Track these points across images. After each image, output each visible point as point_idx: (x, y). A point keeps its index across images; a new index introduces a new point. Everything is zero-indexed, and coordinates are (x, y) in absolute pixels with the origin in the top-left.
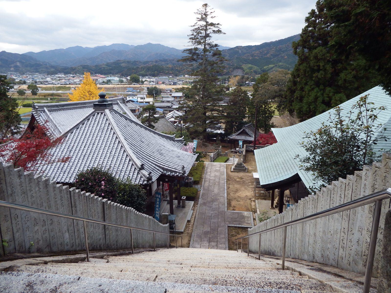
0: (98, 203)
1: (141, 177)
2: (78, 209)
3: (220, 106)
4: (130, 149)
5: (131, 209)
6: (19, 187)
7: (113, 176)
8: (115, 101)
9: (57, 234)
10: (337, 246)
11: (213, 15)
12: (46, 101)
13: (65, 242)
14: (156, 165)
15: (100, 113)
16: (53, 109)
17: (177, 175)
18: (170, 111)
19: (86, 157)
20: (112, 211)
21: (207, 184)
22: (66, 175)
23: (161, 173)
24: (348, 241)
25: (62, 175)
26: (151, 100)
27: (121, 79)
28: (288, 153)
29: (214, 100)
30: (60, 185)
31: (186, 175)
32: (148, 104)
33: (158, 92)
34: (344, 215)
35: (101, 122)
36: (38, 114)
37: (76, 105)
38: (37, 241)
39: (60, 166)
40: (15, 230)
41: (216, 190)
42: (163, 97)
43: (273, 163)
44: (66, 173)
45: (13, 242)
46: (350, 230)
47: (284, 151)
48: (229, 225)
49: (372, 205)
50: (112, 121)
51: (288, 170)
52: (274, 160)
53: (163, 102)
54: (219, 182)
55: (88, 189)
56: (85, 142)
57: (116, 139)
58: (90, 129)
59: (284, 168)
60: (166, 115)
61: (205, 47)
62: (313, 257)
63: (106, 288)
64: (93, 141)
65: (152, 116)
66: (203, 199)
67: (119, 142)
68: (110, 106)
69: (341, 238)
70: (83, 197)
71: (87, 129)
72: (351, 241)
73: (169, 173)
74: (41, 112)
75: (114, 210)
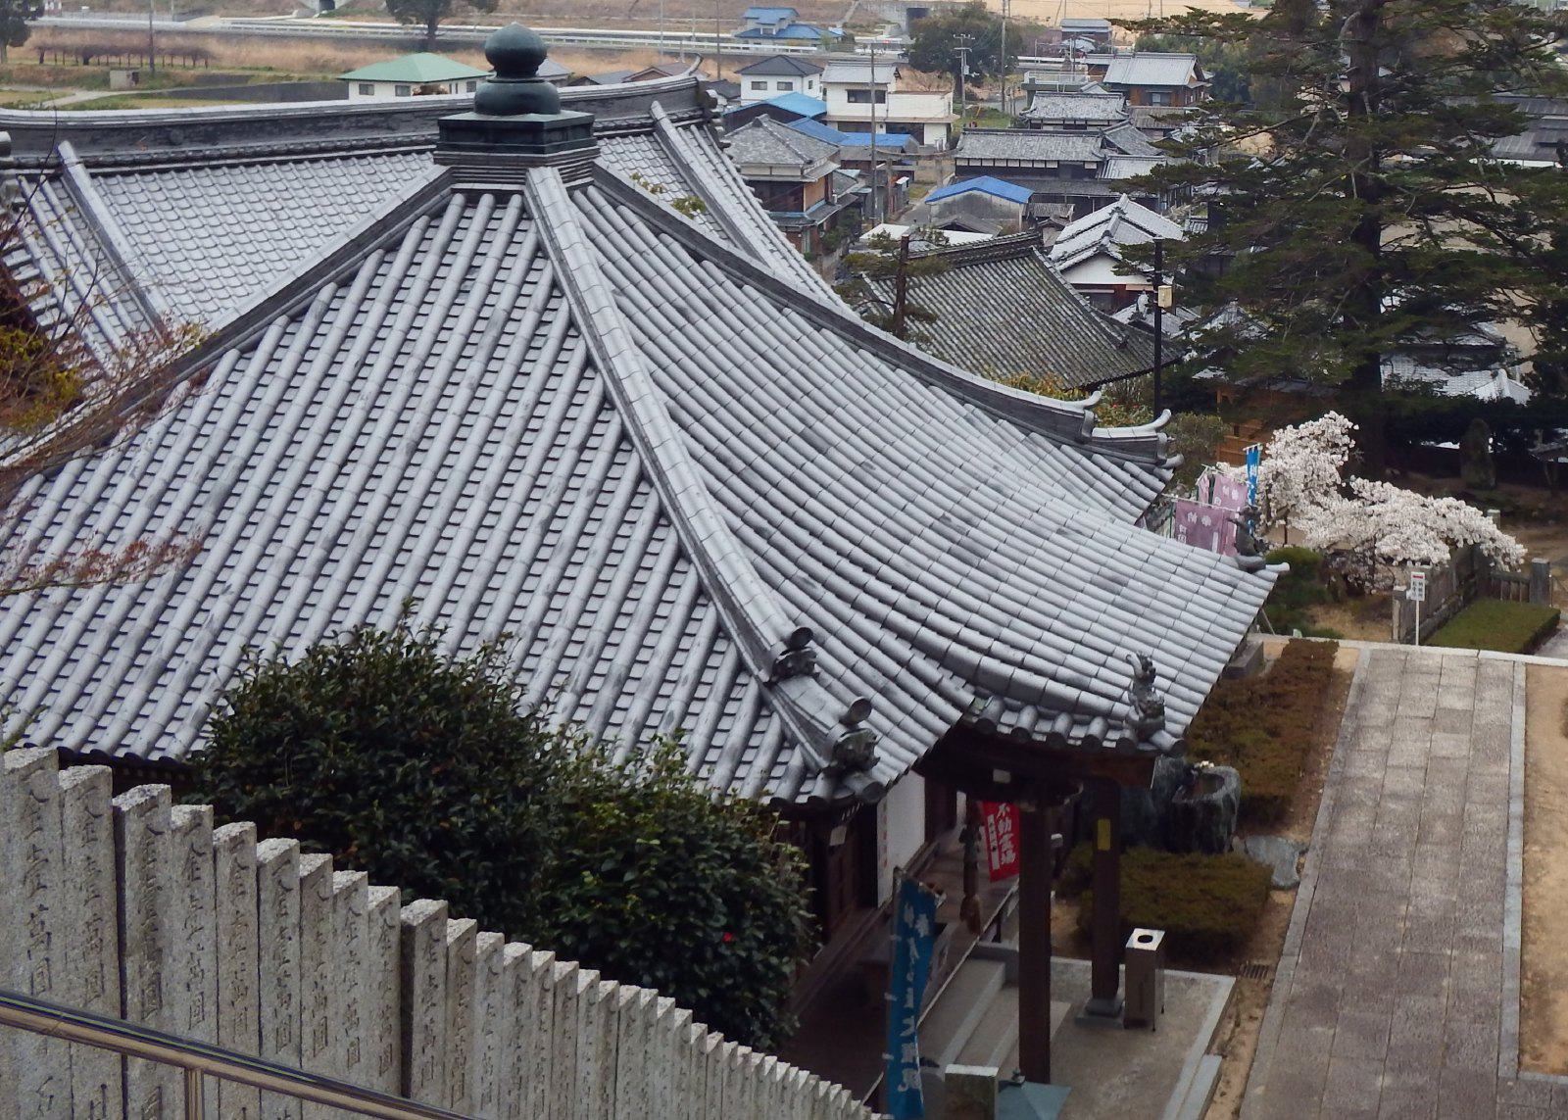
0: (361, 926)
2: (175, 969)
3: (1495, 177)
5: (652, 1004)
7: (523, 713)
8: (628, 110)
12: (94, 95)
14: (916, 643)
15: (487, 201)
16: (125, 152)
17: (1089, 739)
18: (1084, 206)
19: (346, 558)
20: (480, 1011)
21: (1353, 829)
22: (166, 699)
23: (956, 715)
25: (133, 696)
29: (1456, 121)
30: (85, 772)
31: (1166, 739)
32: (903, 139)
33: (994, 45)
35: (487, 266)
37: (319, 131)
39: (125, 618)
41: (1430, 891)
42: (1032, 90)
44: (174, 682)
50: (581, 258)
53: (1032, 127)
54: (1460, 819)
55: (309, 811)
56: (349, 429)
57: (600, 409)
58: (400, 323)
60: (1047, 237)
64: (417, 419)
67: (624, 436)
68: (571, 140)
70: (225, 867)
71: (370, 322)
73: (1025, 719)
74: (31, 179)
75: (495, 999)
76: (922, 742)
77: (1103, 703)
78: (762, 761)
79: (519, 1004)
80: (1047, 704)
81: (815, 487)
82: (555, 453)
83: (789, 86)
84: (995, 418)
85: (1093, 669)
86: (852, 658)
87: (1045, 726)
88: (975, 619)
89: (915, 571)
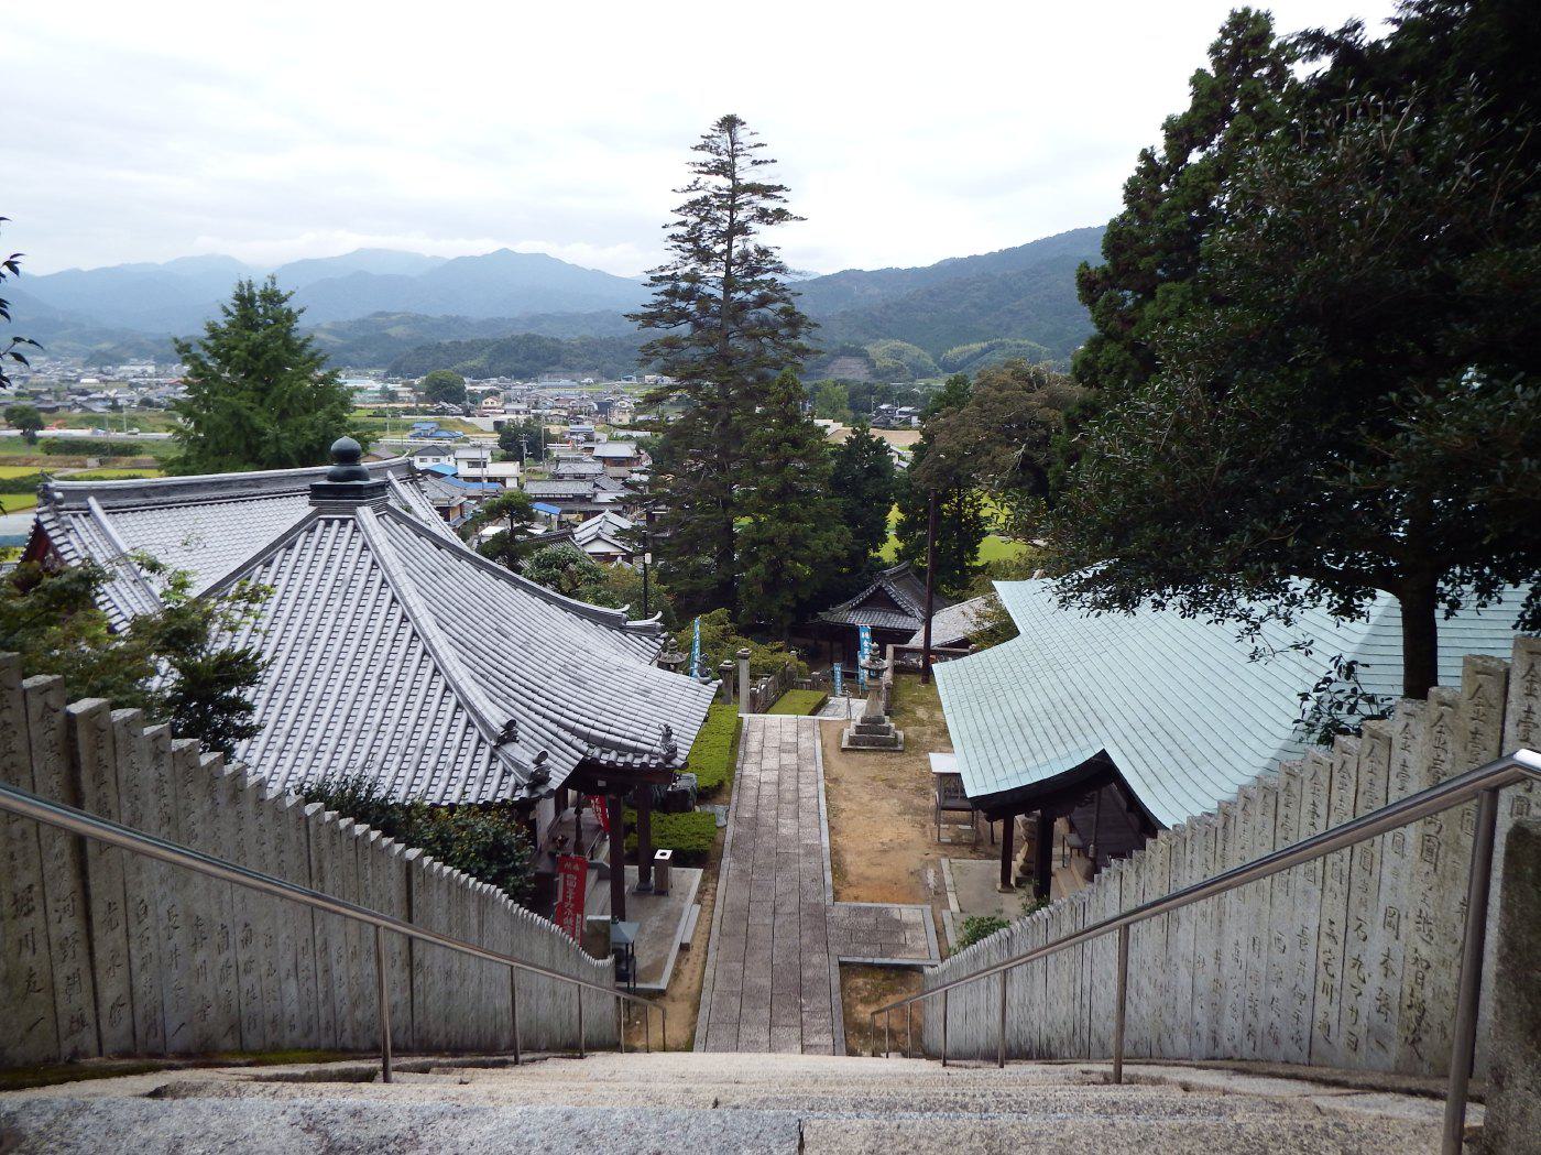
1: (504, 771)
4: (457, 663)
6: (152, 797)
9: (264, 983)
10: (1306, 988)
11: (759, 154)
13: (287, 1016)
15: (336, 523)
17: (643, 764)
18: (587, 516)
20: (436, 897)
23: (581, 756)
24: (1346, 967)
26: (510, 469)
27: (390, 386)
28: (1061, 674)
32: (499, 485)
34: (1328, 874)
36: (64, 523)
38: (198, 1007)
40: (137, 963)
42: (558, 461)
43: (1007, 712)
45: (128, 1007)
46: (1356, 928)
47: (1031, 675)
48: (844, 959)
49: (1471, 806)
50: (387, 551)
51: (1067, 739)
52: (1014, 703)
53: (559, 477)
59: (1052, 732)
61: (728, 272)
62: (1211, 1042)
63: (593, 1126)
65: (522, 530)
66: (737, 859)
69: (1323, 958)
72: (1358, 964)
73: (613, 756)
74: (75, 516)
76: (567, 770)
77: (648, 748)
78: (495, 782)
79: (449, 894)
80: (622, 749)
81: (505, 655)
82: (381, 643)
83: (438, 460)
84: (581, 618)
85: (642, 732)
86: (532, 733)
87: (621, 759)
88: (585, 712)
89: (556, 691)
